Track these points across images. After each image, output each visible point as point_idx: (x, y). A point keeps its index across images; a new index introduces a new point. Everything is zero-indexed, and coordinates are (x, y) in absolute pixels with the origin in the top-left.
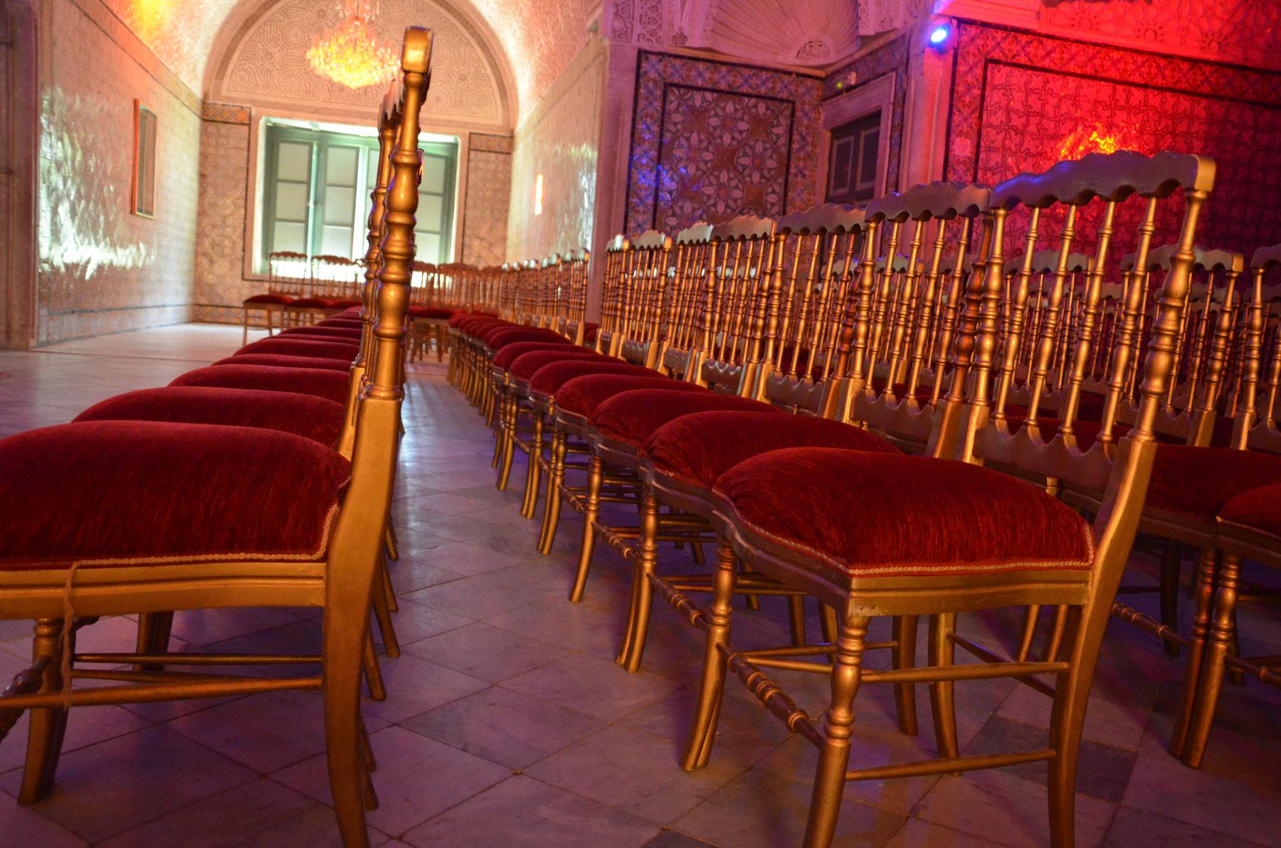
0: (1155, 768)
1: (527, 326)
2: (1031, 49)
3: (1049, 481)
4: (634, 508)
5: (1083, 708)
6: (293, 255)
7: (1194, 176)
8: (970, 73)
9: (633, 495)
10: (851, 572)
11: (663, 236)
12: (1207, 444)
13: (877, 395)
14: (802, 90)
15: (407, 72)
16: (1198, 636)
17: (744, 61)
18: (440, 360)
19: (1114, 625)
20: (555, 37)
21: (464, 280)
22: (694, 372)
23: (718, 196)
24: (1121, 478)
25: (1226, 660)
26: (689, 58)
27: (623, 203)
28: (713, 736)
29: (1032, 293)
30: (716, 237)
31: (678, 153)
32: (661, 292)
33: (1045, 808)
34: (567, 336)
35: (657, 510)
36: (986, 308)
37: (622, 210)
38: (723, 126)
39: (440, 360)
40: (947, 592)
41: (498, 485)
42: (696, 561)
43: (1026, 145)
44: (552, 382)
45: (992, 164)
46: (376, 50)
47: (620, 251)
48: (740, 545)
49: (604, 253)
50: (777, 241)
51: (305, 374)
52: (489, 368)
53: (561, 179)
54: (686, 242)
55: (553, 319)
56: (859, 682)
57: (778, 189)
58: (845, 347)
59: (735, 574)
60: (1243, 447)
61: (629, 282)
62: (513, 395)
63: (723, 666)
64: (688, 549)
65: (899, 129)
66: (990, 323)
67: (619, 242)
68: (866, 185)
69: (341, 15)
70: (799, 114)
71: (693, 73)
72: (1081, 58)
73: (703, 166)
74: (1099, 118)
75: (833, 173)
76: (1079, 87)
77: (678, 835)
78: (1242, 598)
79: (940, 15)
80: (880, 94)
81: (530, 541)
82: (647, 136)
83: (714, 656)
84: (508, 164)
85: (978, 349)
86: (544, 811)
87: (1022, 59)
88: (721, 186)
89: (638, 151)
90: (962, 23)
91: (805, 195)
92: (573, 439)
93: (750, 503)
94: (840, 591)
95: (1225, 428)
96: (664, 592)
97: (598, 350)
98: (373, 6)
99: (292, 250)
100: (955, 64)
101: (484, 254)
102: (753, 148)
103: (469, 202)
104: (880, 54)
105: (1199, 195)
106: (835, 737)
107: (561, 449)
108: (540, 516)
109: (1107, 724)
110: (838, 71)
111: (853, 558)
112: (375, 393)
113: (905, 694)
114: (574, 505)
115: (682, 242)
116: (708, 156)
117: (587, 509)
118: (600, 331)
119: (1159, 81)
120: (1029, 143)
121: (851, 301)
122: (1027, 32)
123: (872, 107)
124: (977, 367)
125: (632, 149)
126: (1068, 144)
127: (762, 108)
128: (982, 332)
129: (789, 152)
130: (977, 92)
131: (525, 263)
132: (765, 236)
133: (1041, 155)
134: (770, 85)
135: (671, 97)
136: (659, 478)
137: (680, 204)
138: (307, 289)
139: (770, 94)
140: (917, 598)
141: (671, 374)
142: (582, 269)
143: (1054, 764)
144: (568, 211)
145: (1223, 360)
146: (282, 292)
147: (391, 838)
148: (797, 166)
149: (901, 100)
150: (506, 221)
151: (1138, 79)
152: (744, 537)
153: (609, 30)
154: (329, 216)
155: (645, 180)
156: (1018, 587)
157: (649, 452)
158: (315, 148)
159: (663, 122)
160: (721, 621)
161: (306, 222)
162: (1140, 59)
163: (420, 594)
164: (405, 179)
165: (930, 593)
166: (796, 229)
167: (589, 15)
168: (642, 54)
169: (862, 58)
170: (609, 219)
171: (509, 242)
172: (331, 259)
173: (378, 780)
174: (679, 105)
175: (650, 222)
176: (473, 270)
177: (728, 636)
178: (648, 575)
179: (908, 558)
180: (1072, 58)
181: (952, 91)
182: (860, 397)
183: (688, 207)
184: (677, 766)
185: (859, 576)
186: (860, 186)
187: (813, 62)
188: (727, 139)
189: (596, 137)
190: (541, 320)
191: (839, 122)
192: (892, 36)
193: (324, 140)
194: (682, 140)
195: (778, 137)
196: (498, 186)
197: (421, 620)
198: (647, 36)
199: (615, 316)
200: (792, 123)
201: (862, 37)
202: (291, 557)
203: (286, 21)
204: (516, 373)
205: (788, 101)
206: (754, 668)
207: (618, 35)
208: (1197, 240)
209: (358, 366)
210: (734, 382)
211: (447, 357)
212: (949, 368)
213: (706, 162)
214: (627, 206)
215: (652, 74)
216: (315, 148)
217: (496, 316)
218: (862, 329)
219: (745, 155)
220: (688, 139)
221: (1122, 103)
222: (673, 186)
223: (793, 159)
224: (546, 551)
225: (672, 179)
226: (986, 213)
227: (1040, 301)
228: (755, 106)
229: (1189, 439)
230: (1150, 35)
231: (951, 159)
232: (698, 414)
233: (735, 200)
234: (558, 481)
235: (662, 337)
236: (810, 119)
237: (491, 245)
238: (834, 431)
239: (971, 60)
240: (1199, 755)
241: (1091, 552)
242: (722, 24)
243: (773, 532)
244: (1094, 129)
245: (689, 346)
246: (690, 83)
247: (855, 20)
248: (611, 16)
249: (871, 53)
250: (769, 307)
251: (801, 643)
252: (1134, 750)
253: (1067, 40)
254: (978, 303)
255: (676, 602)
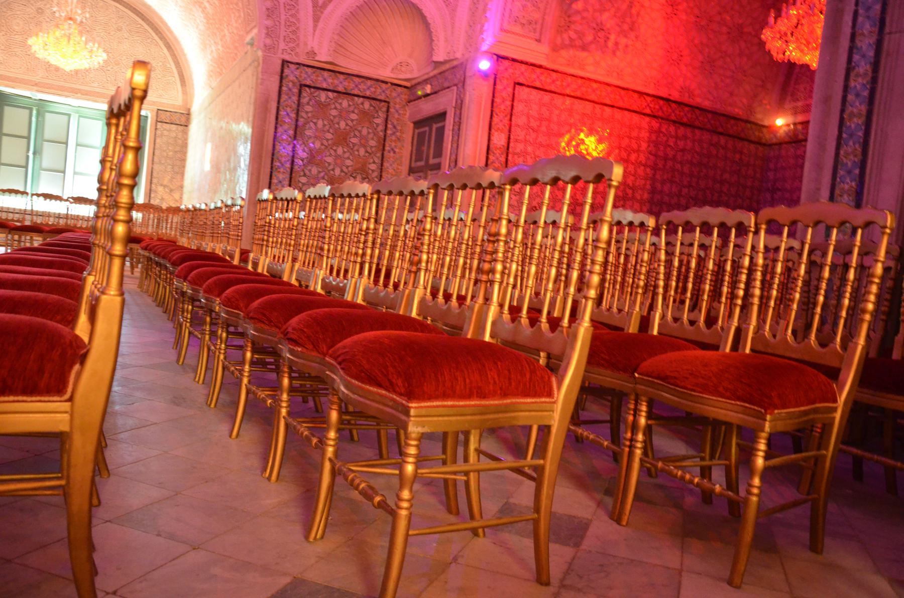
0: (601, 527)
1: (198, 249)
2: (542, 78)
3: (542, 354)
4: (273, 376)
5: (553, 487)
6: (16, 192)
7: (611, 172)
8: (504, 91)
9: (274, 367)
10: (410, 405)
11: (296, 192)
12: (636, 331)
13: (446, 302)
14: (394, 94)
15: (133, 89)
16: (625, 446)
17: (355, 73)
18: (132, 273)
19: (573, 441)
20: (222, 46)
21: (152, 216)
22: (316, 283)
23: (336, 164)
24: (573, 348)
25: (641, 460)
26: (318, 68)
27: (270, 166)
28: (327, 519)
29: (545, 236)
30: (332, 195)
31: (308, 133)
32: (294, 229)
33: (533, 555)
34: (227, 258)
35: (290, 374)
36: (498, 245)
37: (268, 170)
38: (340, 116)
39: (132, 273)
40: (469, 417)
41: (178, 361)
42: (317, 411)
43: (540, 139)
44: (219, 289)
45: (518, 150)
46: (86, 43)
47: (266, 201)
48: (343, 393)
49: (254, 200)
50: (371, 199)
51: (42, 280)
52: (171, 280)
53: (224, 146)
54: (312, 196)
55: (218, 246)
56: (416, 475)
57: (377, 160)
58: (414, 269)
59: (341, 412)
60: (655, 332)
61: (273, 222)
62: (189, 298)
63: (334, 473)
64: (310, 395)
65: (458, 124)
66: (500, 255)
67: (266, 194)
68: (436, 161)
69: (57, 15)
70: (392, 110)
71: (320, 78)
72: (574, 86)
73: (325, 142)
74: (584, 124)
75: (414, 151)
76: (572, 104)
77: (304, 580)
78: (649, 422)
79: (486, 52)
80: (445, 101)
81: (201, 399)
82: (287, 120)
83: (327, 466)
84: (186, 133)
85: (493, 271)
86: (216, 570)
87: (538, 84)
88: (337, 157)
89: (280, 130)
90: (500, 58)
91: (395, 166)
92: (232, 329)
93: (349, 365)
94: (404, 418)
95: (645, 322)
96: (295, 427)
97: (250, 267)
98: (83, 8)
99: (16, 188)
100: (495, 84)
101: (166, 197)
102: (360, 132)
103: (156, 159)
104: (447, 74)
105: (615, 183)
106: (401, 508)
107: (224, 335)
108: (208, 383)
109: (570, 501)
110: (419, 83)
111: (411, 395)
112: (107, 292)
113: (451, 488)
114: (233, 373)
115: (309, 197)
116: (329, 136)
117: (242, 375)
118: (252, 255)
119: (621, 104)
120: (542, 139)
121: (418, 239)
122: (540, 67)
123: (440, 109)
124: (492, 282)
125: (276, 128)
126: (566, 139)
127: (367, 105)
128: (495, 260)
129: (385, 136)
130: (509, 103)
131: (198, 206)
132: (364, 195)
133: (548, 145)
134: (373, 89)
135: (304, 94)
136: (292, 352)
137: (309, 168)
138: (28, 217)
139: (373, 96)
140: (451, 421)
141: (300, 285)
142: (239, 212)
143: (536, 522)
144: (229, 170)
145: (869, 293)
146: (7, 219)
147: (108, 593)
148: (390, 146)
149: (460, 105)
150: (182, 174)
151: (608, 102)
152: (346, 387)
153: (262, 45)
154: (46, 163)
155: (285, 151)
156: (513, 414)
157: (285, 335)
158: (34, 112)
159: (298, 110)
160: (332, 443)
161: (26, 167)
162: (609, 89)
163: (122, 436)
164: (130, 156)
165: (459, 418)
166: (384, 191)
167: (248, 33)
168: (285, 63)
169: (435, 76)
170: (259, 174)
171: (185, 190)
172: (47, 196)
173: (97, 557)
174: (310, 100)
175: (287, 183)
176: (157, 209)
177: (336, 453)
178: (284, 417)
179: (445, 396)
180: (568, 85)
181: (493, 102)
182: (422, 301)
183: (315, 170)
184: (303, 539)
185: (415, 408)
186: (432, 161)
187: (401, 77)
188: (343, 125)
189: (251, 119)
190: (209, 246)
191: (419, 117)
192: (455, 63)
193: (42, 107)
194: (311, 124)
195: (378, 125)
196: (178, 148)
197: (122, 454)
198: (289, 51)
199: (262, 245)
200: (387, 116)
201: (436, 62)
202: (46, 399)
203: (10, 13)
204: (193, 283)
205: (385, 101)
206: (353, 471)
207: (268, 49)
208: (615, 206)
209: (89, 274)
210: (342, 291)
211: (138, 271)
212: (476, 282)
213: (327, 140)
214: (272, 168)
215: (292, 78)
216: (34, 112)
217: (175, 242)
218: (425, 257)
219: (355, 136)
220: (315, 124)
221: (599, 116)
222: (304, 155)
223: (388, 139)
224: (213, 405)
225: (304, 151)
226: (499, 187)
227: (549, 241)
228: (362, 104)
229: (626, 328)
230: (615, 74)
231: (491, 146)
232: (317, 311)
233: (347, 167)
234: (222, 357)
235: (294, 260)
236: (399, 114)
237: (171, 190)
238: (406, 322)
239: (505, 82)
240: (626, 518)
241: (556, 392)
242: (341, 46)
243: (363, 382)
244: (582, 131)
245: (313, 266)
246: (318, 86)
247: (431, 51)
248: (263, 35)
249: (440, 73)
250: (365, 242)
251: (385, 456)
252: (590, 518)
253: (565, 74)
254: (494, 242)
255: (302, 433)
